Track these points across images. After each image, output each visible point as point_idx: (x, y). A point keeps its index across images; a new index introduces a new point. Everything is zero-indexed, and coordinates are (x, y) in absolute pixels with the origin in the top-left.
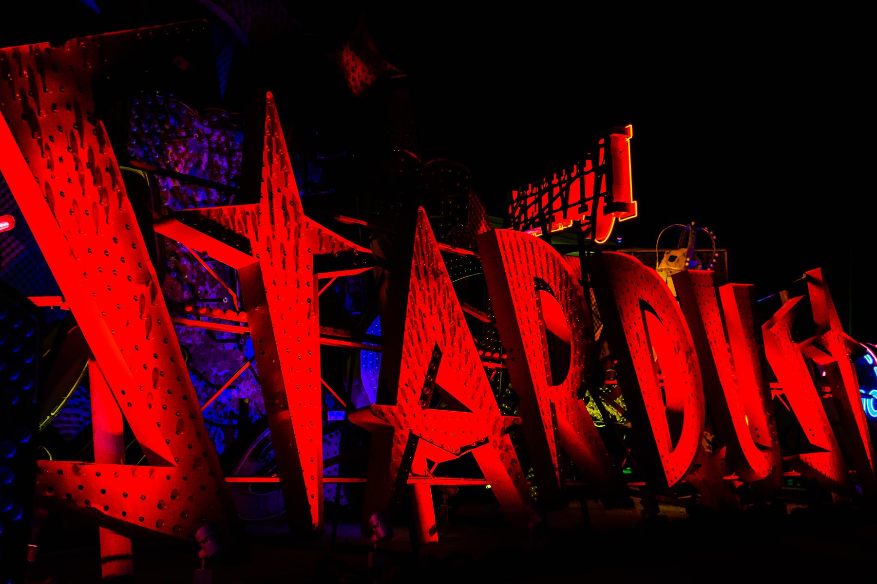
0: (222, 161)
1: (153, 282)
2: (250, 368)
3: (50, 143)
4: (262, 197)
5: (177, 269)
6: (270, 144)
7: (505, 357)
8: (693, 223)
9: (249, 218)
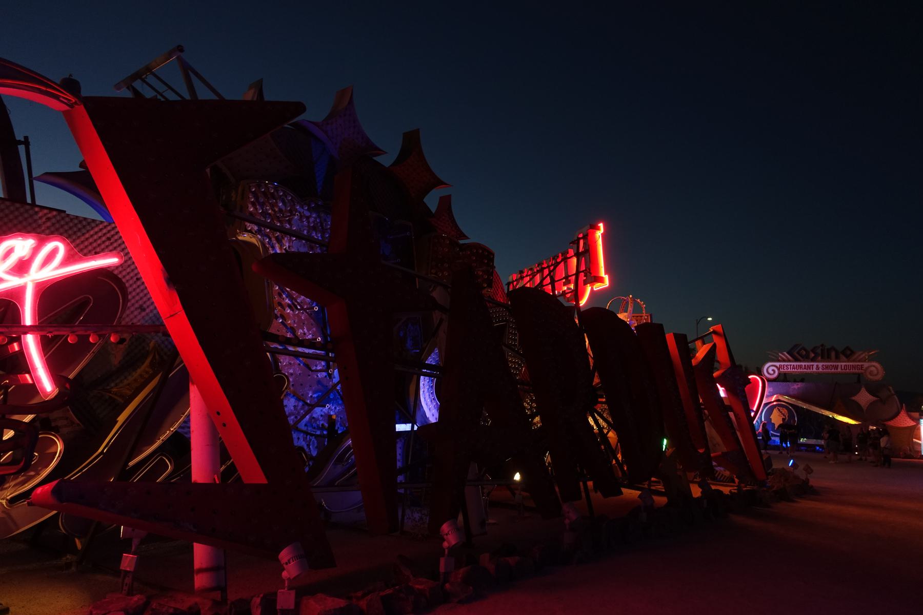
5: (282, 317)
8: (631, 296)
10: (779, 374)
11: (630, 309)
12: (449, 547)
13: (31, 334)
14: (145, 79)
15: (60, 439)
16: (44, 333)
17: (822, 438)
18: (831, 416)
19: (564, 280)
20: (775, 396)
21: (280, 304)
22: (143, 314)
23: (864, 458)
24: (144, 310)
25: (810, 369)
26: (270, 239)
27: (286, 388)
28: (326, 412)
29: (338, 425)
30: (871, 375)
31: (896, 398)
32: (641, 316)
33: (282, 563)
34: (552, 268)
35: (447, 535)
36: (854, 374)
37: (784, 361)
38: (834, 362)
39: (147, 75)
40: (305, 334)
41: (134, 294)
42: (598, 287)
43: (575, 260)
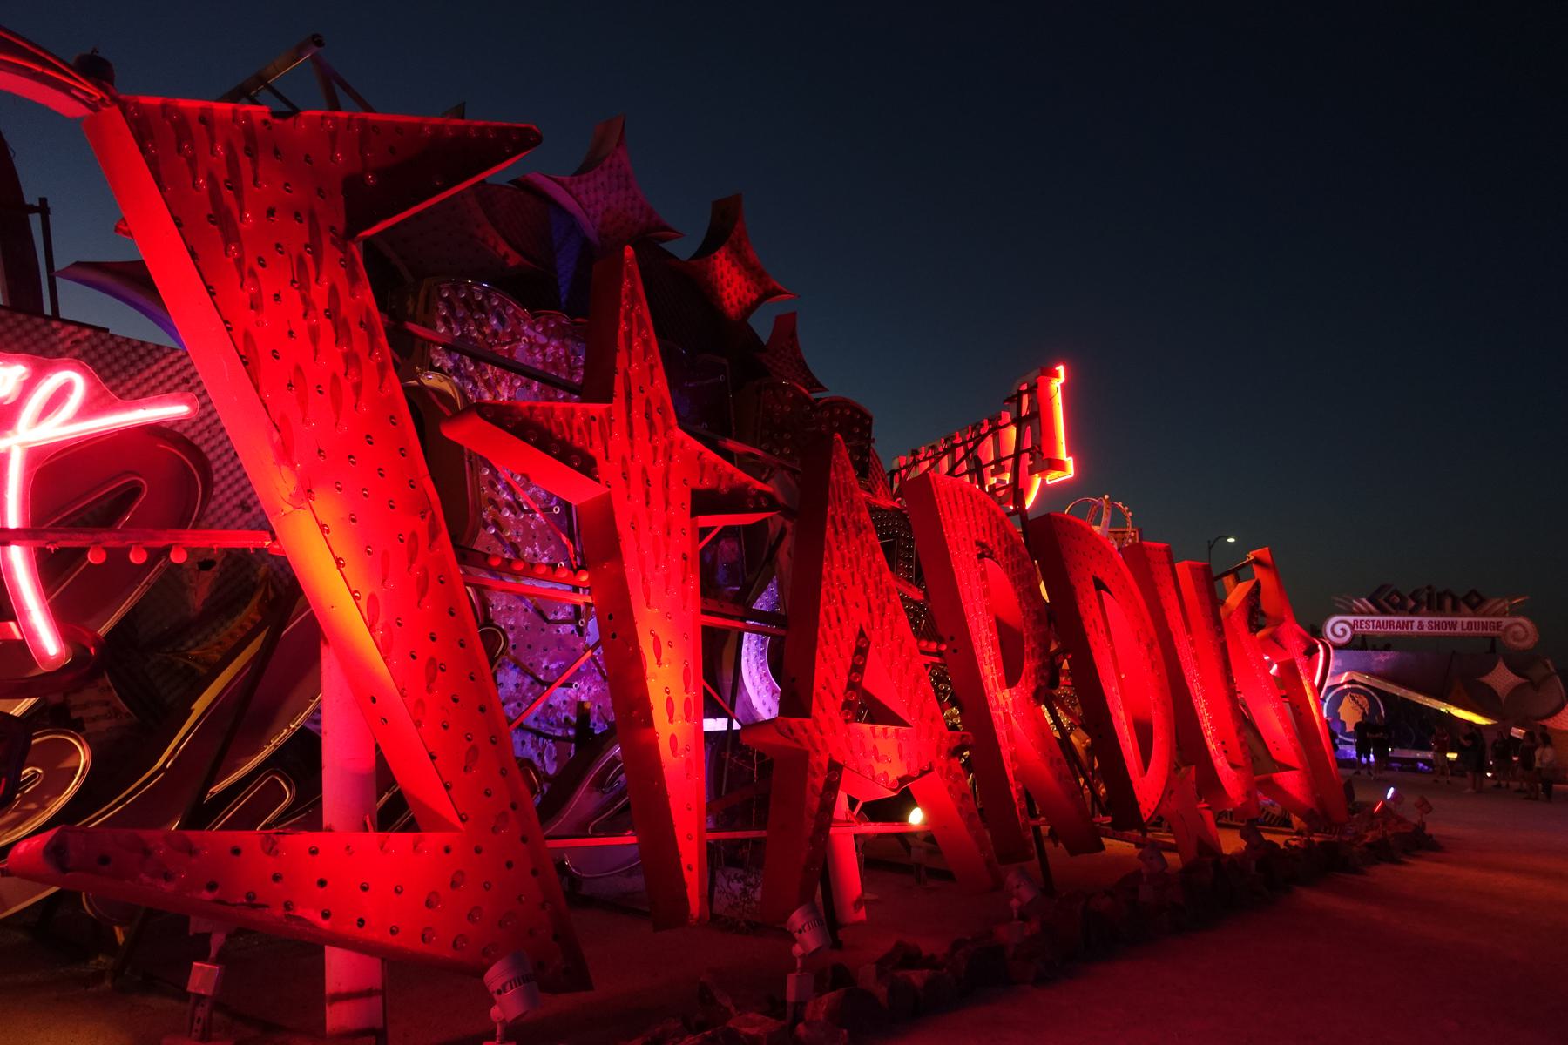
1: (433, 513)
2: (593, 657)
3: (258, 269)
4: (615, 396)
5: (496, 524)
6: (628, 318)
7: (944, 647)
9: (595, 425)
10: (1354, 637)
12: (804, 954)
13: (18, 545)
14: (256, 98)
15: (85, 748)
16: (40, 543)
17: (1429, 749)
18: (1444, 710)
19: (993, 467)
20: (1346, 674)
21: (492, 502)
22: (247, 516)
23: (1504, 783)
24: (248, 509)
25: (1407, 628)
26: (475, 384)
27: (502, 653)
28: (573, 696)
29: (594, 719)
30: (1515, 640)
31: (1559, 679)
33: (491, 991)
34: (970, 445)
36: (1485, 637)
37: (1361, 613)
38: (1451, 616)
39: (258, 91)
40: (536, 555)
41: (224, 472)
42: (1054, 478)
43: (1013, 431)
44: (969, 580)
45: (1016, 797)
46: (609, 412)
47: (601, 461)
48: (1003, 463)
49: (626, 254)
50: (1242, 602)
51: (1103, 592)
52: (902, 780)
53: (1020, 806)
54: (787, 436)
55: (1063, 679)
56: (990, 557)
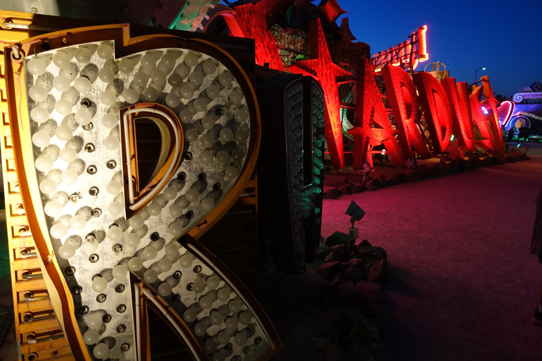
0: (292, 47)
11: (438, 69)
19: (404, 57)
32: (443, 72)
35: (365, 167)
37: (527, 92)
42: (422, 60)
43: (410, 46)
44: (398, 92)
45: (409, 145)
46: (318, 61)
47: (318, 73)
48: (407, 56)
49: (318, 20)
50: (477, 92)
51: (435, 93)
52: (383, 141)
53: (410, 147)
54: (348, 55)
55: (422, 117)
56: (403, 86)
